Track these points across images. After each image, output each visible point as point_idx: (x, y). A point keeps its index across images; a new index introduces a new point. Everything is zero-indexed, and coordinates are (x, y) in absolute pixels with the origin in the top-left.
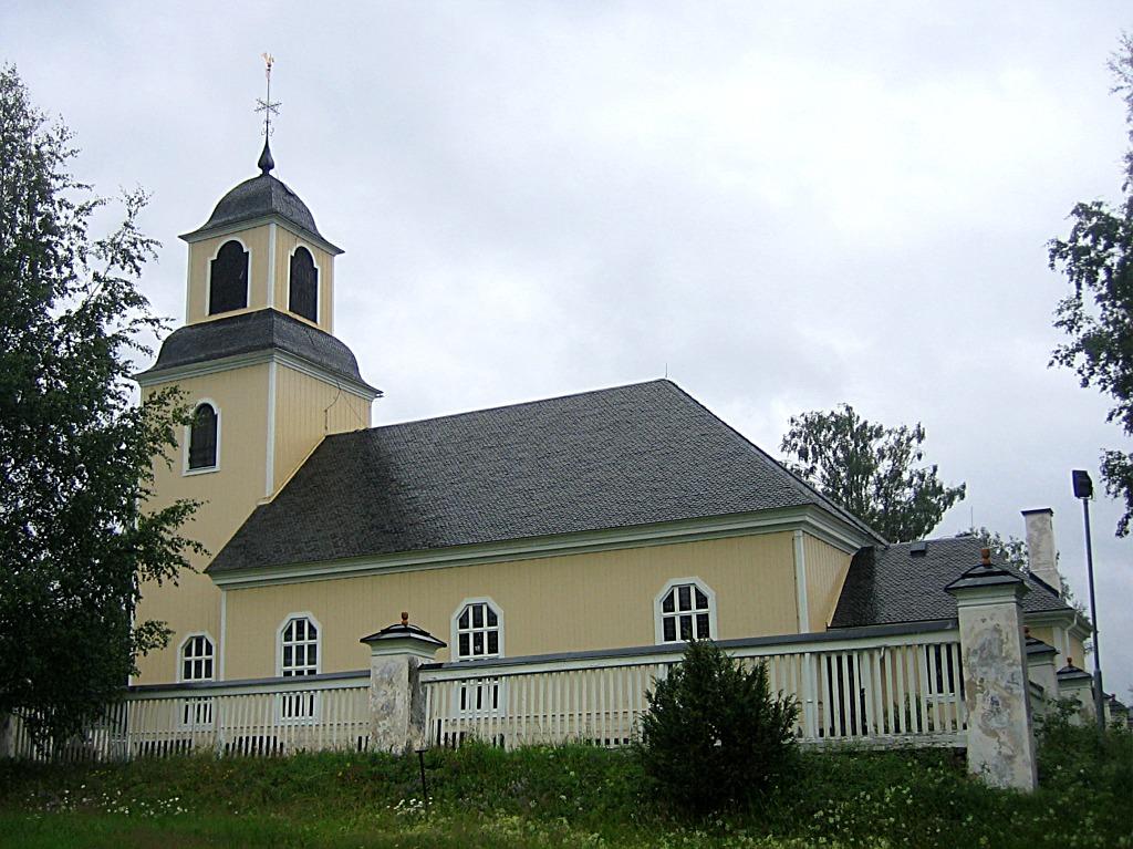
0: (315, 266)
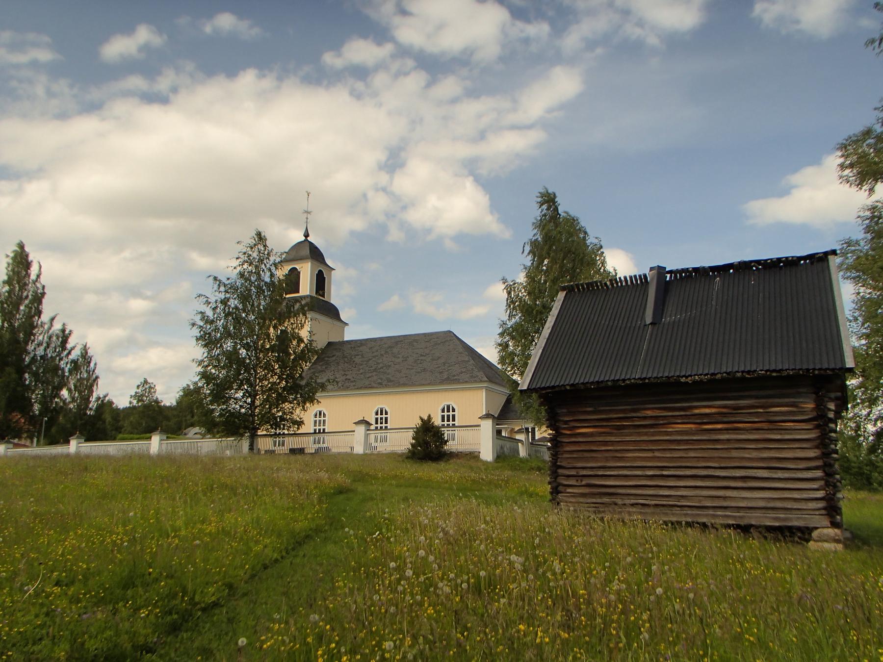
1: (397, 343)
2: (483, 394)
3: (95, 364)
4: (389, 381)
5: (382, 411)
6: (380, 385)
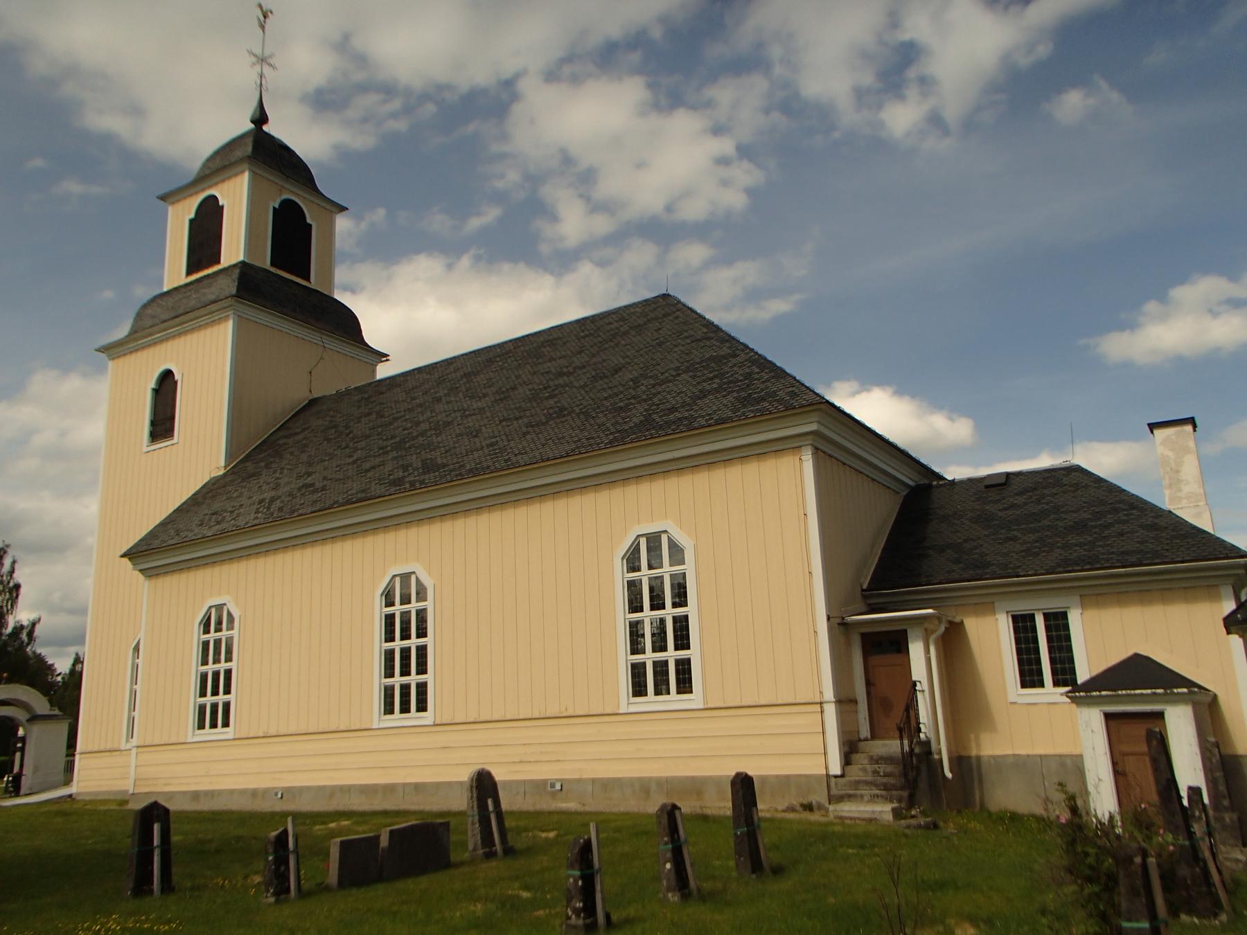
0: (309, 221)
2: (807, 463)
3: (14, 562)
4: (428, 467)
6: (399, 486)
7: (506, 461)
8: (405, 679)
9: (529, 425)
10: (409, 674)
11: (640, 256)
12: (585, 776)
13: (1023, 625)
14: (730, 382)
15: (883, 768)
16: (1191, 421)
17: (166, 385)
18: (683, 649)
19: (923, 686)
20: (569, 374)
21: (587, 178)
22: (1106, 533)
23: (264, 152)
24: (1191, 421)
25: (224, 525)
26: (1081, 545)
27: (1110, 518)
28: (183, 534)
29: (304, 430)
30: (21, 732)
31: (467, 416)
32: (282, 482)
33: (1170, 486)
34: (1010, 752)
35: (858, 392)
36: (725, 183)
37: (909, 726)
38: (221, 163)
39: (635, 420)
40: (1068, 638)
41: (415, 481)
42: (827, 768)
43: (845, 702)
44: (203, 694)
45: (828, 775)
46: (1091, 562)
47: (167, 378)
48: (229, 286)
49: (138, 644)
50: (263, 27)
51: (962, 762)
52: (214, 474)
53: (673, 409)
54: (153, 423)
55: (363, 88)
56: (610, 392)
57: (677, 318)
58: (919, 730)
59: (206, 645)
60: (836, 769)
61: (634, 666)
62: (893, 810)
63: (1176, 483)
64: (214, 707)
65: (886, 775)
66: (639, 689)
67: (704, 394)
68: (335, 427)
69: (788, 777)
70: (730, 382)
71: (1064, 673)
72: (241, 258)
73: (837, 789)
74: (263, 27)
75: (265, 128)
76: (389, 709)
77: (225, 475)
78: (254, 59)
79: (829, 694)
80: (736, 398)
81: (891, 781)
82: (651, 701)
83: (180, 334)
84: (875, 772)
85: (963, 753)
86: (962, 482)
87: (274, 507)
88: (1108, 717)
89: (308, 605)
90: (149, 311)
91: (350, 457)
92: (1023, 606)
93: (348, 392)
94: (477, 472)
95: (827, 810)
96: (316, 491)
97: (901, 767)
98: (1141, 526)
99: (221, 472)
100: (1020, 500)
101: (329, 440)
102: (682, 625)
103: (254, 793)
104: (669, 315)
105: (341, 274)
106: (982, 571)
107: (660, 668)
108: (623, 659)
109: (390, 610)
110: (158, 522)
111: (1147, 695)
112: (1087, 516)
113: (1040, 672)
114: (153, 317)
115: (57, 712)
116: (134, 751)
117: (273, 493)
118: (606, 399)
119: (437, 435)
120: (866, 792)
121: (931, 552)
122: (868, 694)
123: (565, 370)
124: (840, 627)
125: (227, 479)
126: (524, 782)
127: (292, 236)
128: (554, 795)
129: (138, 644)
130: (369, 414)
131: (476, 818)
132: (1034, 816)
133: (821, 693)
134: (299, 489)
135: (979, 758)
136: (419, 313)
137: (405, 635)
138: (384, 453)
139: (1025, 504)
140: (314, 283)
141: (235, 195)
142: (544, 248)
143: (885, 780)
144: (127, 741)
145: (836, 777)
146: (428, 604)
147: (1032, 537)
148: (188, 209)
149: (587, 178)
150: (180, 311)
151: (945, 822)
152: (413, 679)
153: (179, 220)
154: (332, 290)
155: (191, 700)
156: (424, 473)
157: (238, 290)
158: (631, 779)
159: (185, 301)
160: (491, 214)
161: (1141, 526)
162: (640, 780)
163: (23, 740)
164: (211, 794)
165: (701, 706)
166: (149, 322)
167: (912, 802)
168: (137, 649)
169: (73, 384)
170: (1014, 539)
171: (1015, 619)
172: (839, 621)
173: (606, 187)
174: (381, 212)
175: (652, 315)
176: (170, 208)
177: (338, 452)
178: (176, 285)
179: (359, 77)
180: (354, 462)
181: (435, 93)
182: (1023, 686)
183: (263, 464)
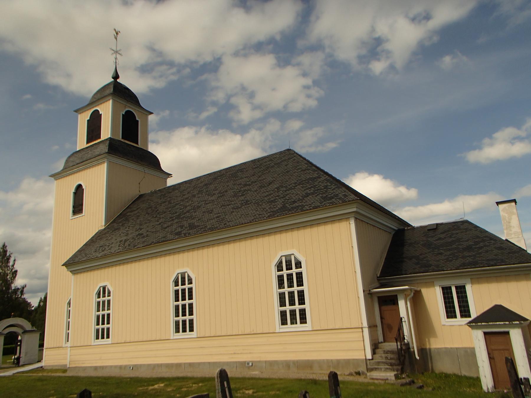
0: (137, 119)
1: (215, 179)
2: (352, 224)
3: (15, 261)
4: (192, 226)
5: (183, 279)
6: (179, 235)
7: (225, 224)
8: (184, 318)
9: (233, 208)
10: (186, 316)
11: (274, 126)
12: (261, 360)
13: (447, 291)
14: (318, 190)
15: (390, 356)
16: (514, 201)
17: (79, 190)
18: (302, 304)
19: (405, 319)
20: (249, 185)
21: (252, 95)
22: (480, 251)
23: (119, 91)
24: (514, 201)
25: (105, 252)
26: (470, 256)
27: (481, 244)
28: (88, 256)
29: (137, 209)
30: (20, 338)
31: (207, 204)
32: (129, 232)
33: (507, 229)
34: (443, 346)
35: (367, 177)
36: (309, 96)
37: (400, 337)
38: (100, 96)
39: (278, 206)
40: (466, 297)
41: (186, 233)
42: (365, 356)
43: (372, 327)
44: (98, 324)
45: (366, 359)
46: (474, 264)
47: (79, 187)
48: (105, 148)
49: (70, 300)
50: (116, 39)
51: (423, 351)
52: (100, 229)
53: (294, 202)
54: (74, 207)
55: (161, 64)
56: (267, 193)
57: (294, 160)
58: (404, 339)
59: (99, 303)
60: (369, 357)
61: (281, 312)
62: (395, 375)
63: (509, 227)
64: (103, 330)
65: (391, 359)
66: (284, 322)
67: (307, 195)
68: (151, 207)
69: (349, 360)
70: (318, 190)
71: (465, 312)
72: (110, 136)
73: (370, 366)
74: (116, 39)
75: (118, 80)
76: (177, 331)
77: (105, 229)
78: (113, 52)
79: (365, 324)
80: (321, 197)
81: (393, 361)
82: (289, 327)
83: (84, 169)
84: (386, 358)
85: (423, 347)
86: (418, 228)
87: (126, 244)
88: (485, 334)
89: (142, 285)
90: (71, 159)
91: (158, 221)
92: (446, 283)
93: (156, 192)
94: (212, 229)
95: (366, 375)
96: (143, 237)
97: (397, 356)
98: (496, 248)
99: (103, 228)
100: (442, 236)
101: (148, 214)
102: (301, 294)
103: (121, 367)
104: (291, 158)
105: (151, 136)
106: (428, 269)
107: (293, 313)
108: (277, 309)
109: (177, 288)
110: (77, 250)
111: (502, 324)
112: (471, 243)
113: (455, 312)
114: (73, 162)
115: (34, 329)
116: (69, 349)
117: (125, 238)
118: (266, 196)
119: (195, 212)
120: (382, 366)
121: (405, 260)
122: (382, 322)
123: (248, 183)
124: (369, 295)
125: (106, 231)
126: (236, 362)
127: (130, 126)
128: (249, 368)
129: (70, 300)
130: (165, 202)
131: (220, 390)
132: (455, 375)
133: (362, 323)
134: (137, 236)
135: (430, 349)
136: (184, 155)
137: (184, 299)
138: (172, 220)
139: (445, 238)
140: (140, 145)
141: (106, 110)
142: (235, 125)
143: (390, 361)
144: (66, 343)
145: (369, 360)
146: (193, 286)
147: (449, 253)
148: (86, 116)
149: (252, 95)
150: (84, 159)
151: (417, 379)
152: (187, 318)
153: (83, 120)
154: (147, 146)
155: (93, 327)
156: (190, 230)
157: (108, 150)
158: (281, 361)
159: (86, 155)
160: (211, 111)
161: (496, 248)
162: (286, 361)
163: (21, 341)
164: (102, 368)
165: (311, 329)
166: (71, 164)
167: (402, 371)
168: (69, 303)
169: (40, 184)
170: (441, 254)
171: (443, 289)
172: (368, 292)
173: (259, 99)
174: (167, 112)
175: (284, 159)
176: (79, 116)
177: (152, 219)
178: (82, 148)
179: (159, 60)
180: (160, 224)
181: (190, 64)
182: (448, 317)
183: (121, 224)
